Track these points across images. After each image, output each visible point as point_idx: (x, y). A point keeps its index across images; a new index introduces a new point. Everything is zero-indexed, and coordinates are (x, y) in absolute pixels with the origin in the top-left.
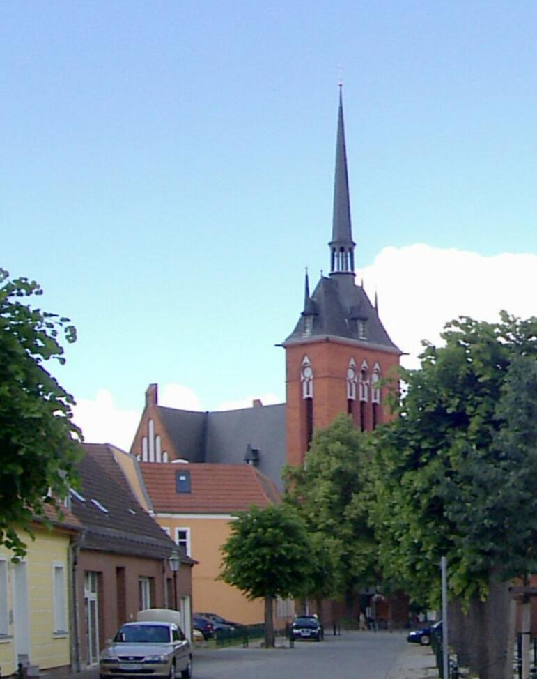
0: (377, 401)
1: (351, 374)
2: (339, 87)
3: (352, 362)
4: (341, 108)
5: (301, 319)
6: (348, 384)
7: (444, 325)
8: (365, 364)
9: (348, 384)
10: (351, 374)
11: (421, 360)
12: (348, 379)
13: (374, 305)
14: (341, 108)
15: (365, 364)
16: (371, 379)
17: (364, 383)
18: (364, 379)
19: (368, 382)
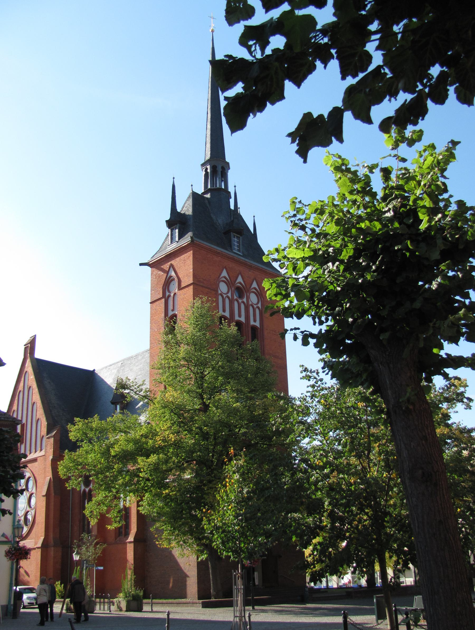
0: (257, 324)
1: (223, 288)
2: (388, 154)
3: (224, 273)
4: (174, 187)
5: (151, 308)
6: (220, 299)
7: (339, 154)
8: (240, 279)
9: (220, 299)
10: (223, 288)
11: (317, 324)
12: (220, 292)
13: (252, 230)
14: (174, 187)
15: (240, 279)
16: (248, 298)
17: (240, 301)
18: (241, 296)
19: (245, 300)
